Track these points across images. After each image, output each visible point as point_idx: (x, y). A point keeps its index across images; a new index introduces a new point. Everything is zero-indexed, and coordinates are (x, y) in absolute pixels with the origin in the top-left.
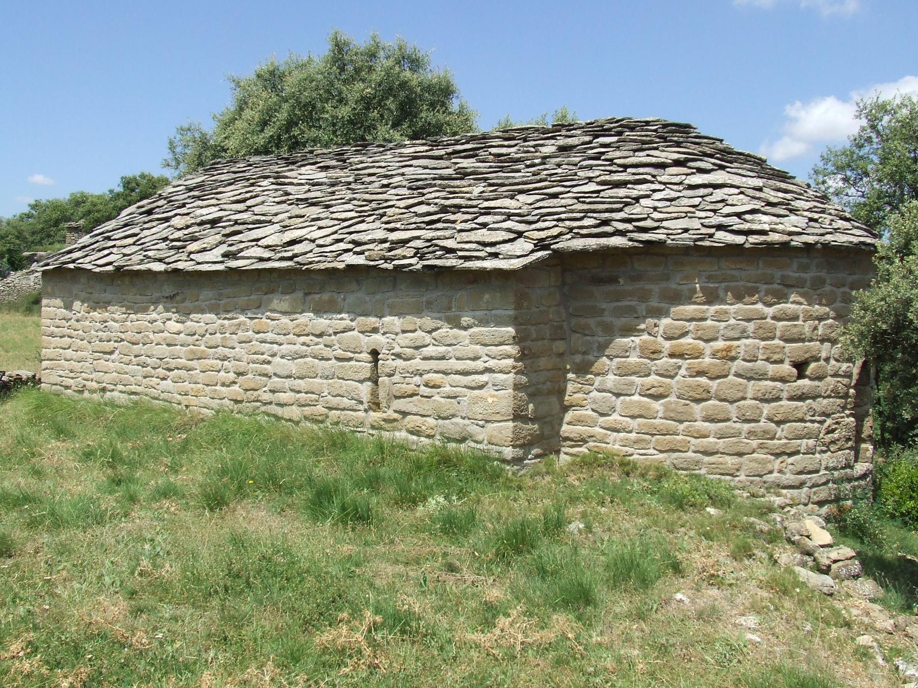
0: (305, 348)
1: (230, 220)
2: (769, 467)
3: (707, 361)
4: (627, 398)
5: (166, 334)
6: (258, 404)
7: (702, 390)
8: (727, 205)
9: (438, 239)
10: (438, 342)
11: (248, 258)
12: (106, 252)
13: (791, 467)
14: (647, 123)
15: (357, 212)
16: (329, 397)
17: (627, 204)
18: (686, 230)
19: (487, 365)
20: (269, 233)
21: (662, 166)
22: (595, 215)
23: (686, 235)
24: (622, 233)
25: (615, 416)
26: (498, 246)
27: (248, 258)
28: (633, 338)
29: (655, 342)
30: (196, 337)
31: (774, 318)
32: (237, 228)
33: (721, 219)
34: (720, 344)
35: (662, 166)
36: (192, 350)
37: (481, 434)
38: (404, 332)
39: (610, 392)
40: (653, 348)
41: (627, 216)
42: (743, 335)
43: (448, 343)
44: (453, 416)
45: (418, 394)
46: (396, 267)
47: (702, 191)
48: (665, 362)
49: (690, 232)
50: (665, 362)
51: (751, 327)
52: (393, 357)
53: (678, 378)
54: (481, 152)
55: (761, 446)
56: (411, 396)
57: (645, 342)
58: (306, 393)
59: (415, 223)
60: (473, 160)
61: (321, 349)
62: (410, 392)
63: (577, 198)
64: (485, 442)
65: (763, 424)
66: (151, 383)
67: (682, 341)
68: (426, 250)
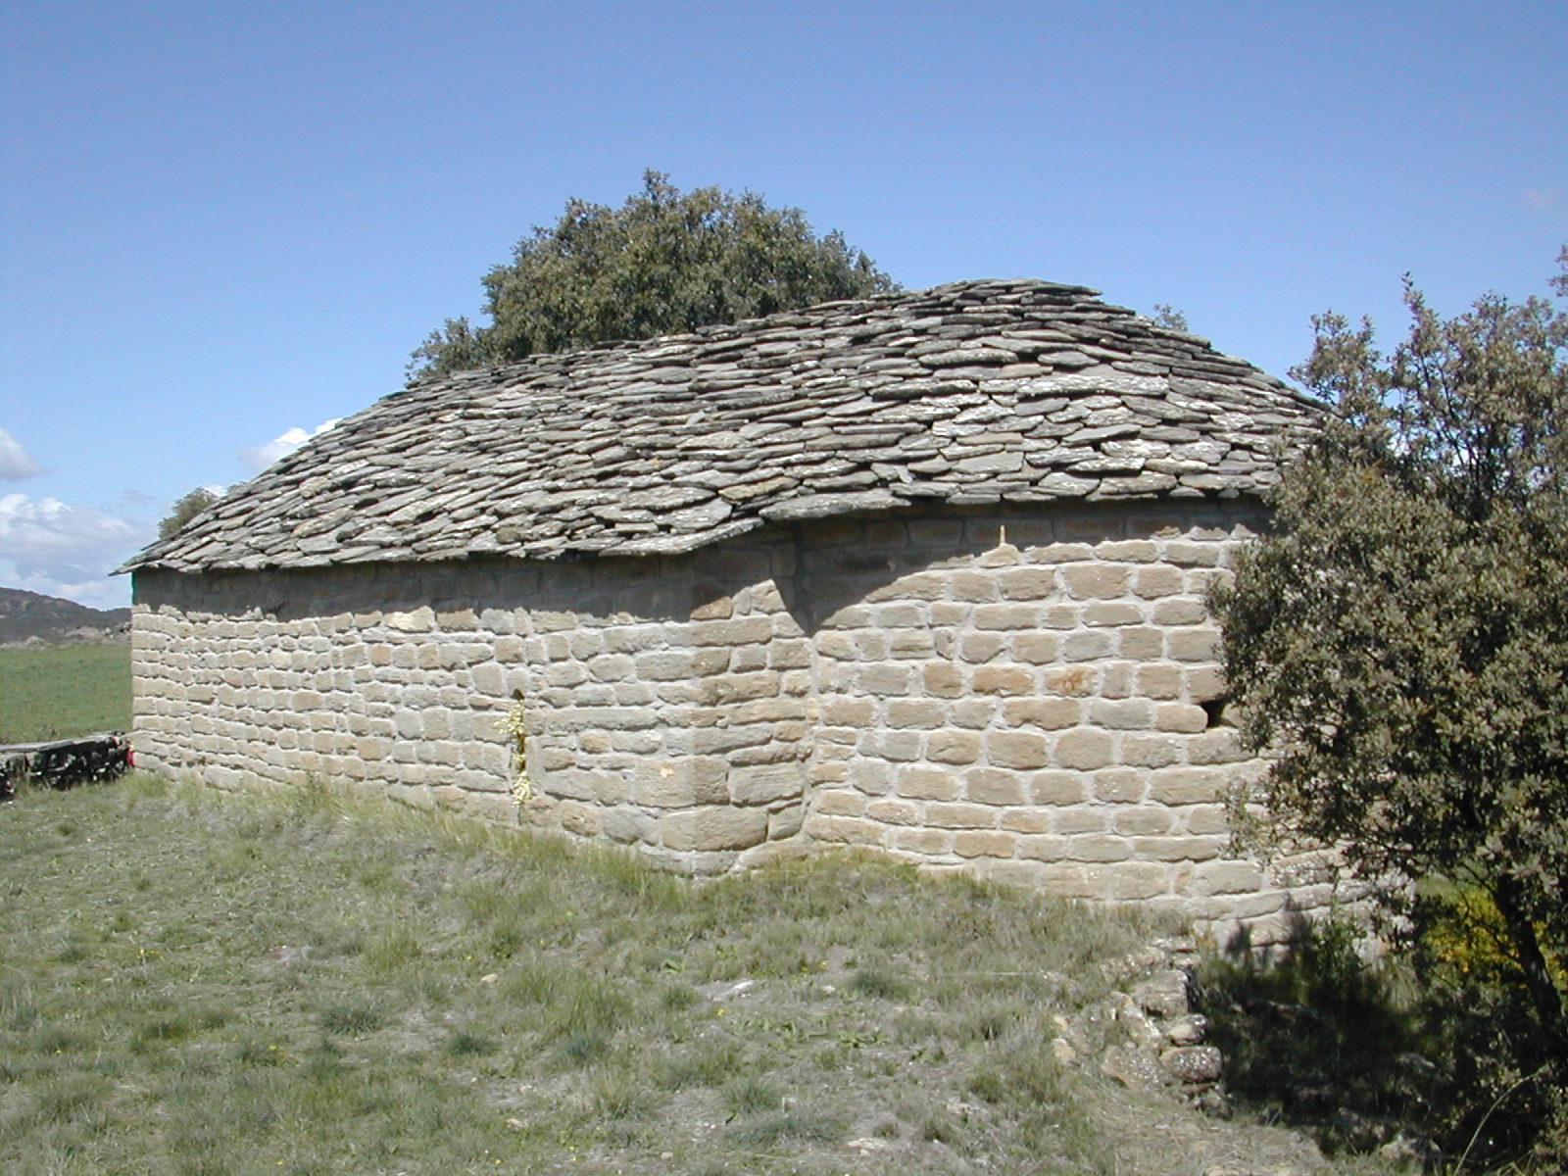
0: (434, 689)
1: (368, 482)
2: (1160, 882)
3: (1039, 698)
4: (908, 766)
5: (271, 670)
6: (383, 781)
7: (1031, 749)
8: (1086, 426)
9: (599, 504)
10: (598, 676)
11: (365, 544)
12: (206, 539)
13: (1200, 883)
14: (1008, 289)
15: (531, 461)
16: (466, 770)
17: (908, 433)
18: (995, 475)
19: (658, 713)
20: (406, 501)
21: (996, 363)
22: (846, 454)
23: (993, 483)
24: (883, 483)
25: (891, 799)
26: (674, 513)
27: (365, 544)
28: (914, 662)
29: (949, 668)
30: (306, 673)
31: (1155, 621)
32: (378, 493)
33: (1066, 451)
34: (1061, 669)
35: (996, 363)
36: (300, 696)
37: (655, 829)
38: (553, 660)
39: (883, 757)
40: (946, 679)
41: (900, 452)
42: (1101, 650)
43: (609, 678)
44: (620, 799)
45: (573, 764)
46: (529, 553)
47: (1051, 403)
48: (968, 700)
49: (1000, 477)
50: (968, 700)
51: (1114, 636)
52: (542, 703)
53: (991, 729)
54: (748, 352)
55: (1142, 847)
56: (566, 767)
57: (931, 669)
58: (438, 764)
59: (582, 478)
60: (734, 365)
61: (453, 691)
62: (564, 761)
63: (831, 426)
64: (661, 843)
65: (1145, 805)
66: (256, 750)
67: (993, 665)
68: (578, 523)
